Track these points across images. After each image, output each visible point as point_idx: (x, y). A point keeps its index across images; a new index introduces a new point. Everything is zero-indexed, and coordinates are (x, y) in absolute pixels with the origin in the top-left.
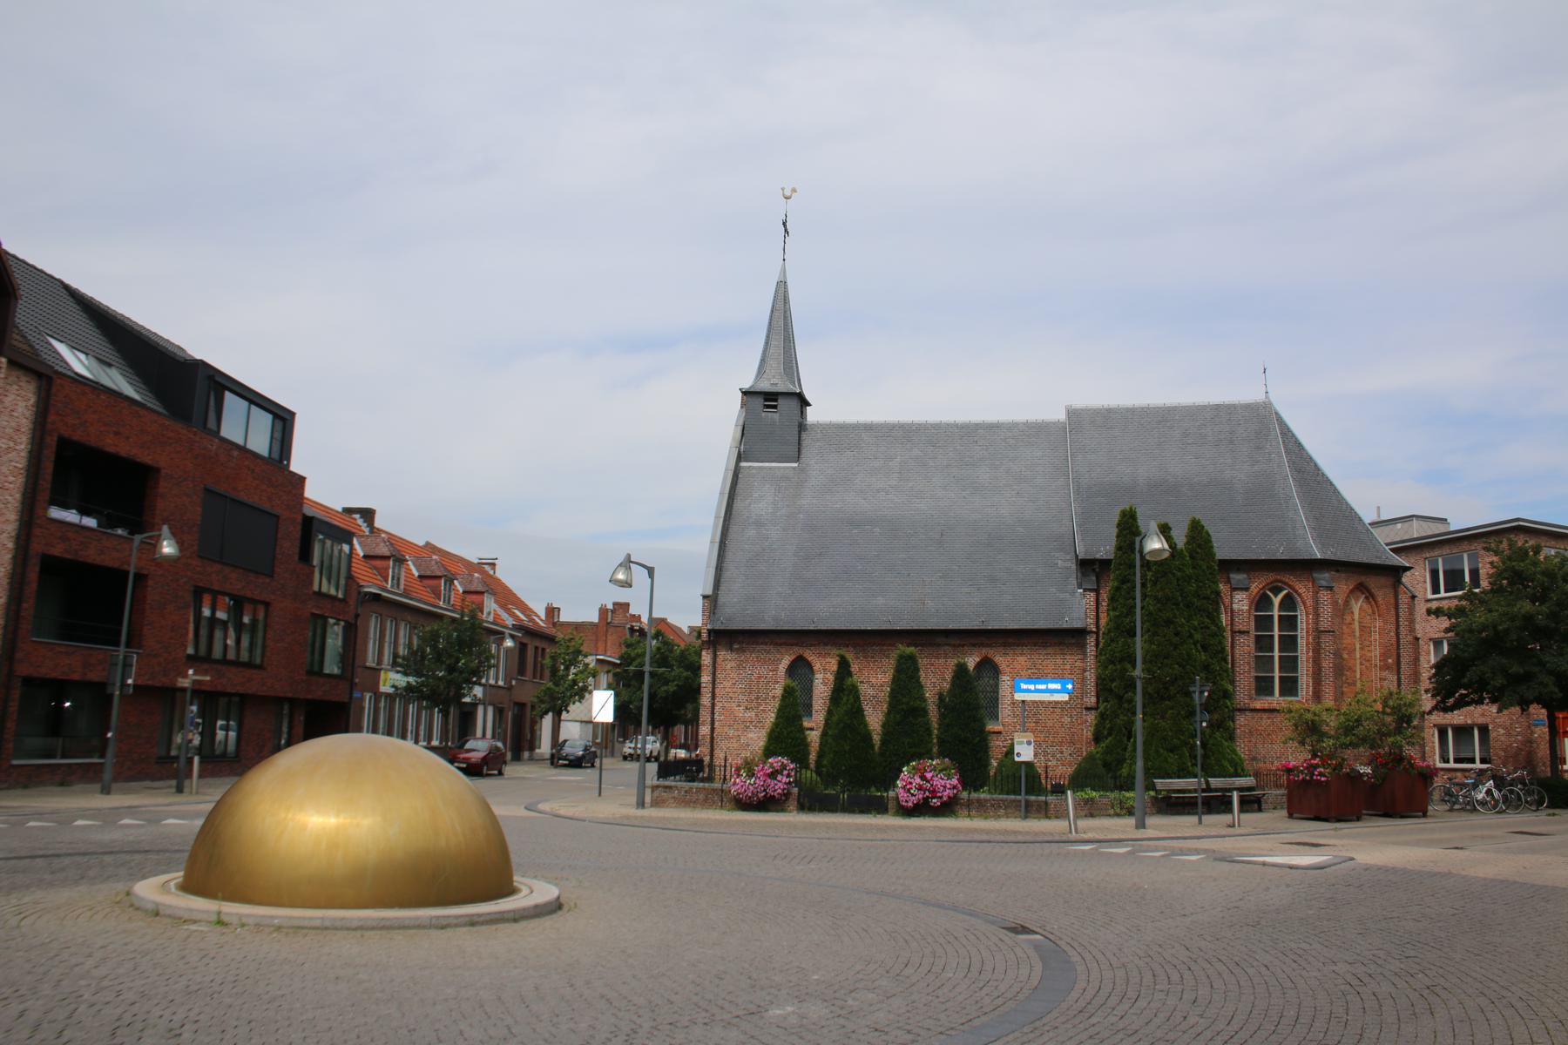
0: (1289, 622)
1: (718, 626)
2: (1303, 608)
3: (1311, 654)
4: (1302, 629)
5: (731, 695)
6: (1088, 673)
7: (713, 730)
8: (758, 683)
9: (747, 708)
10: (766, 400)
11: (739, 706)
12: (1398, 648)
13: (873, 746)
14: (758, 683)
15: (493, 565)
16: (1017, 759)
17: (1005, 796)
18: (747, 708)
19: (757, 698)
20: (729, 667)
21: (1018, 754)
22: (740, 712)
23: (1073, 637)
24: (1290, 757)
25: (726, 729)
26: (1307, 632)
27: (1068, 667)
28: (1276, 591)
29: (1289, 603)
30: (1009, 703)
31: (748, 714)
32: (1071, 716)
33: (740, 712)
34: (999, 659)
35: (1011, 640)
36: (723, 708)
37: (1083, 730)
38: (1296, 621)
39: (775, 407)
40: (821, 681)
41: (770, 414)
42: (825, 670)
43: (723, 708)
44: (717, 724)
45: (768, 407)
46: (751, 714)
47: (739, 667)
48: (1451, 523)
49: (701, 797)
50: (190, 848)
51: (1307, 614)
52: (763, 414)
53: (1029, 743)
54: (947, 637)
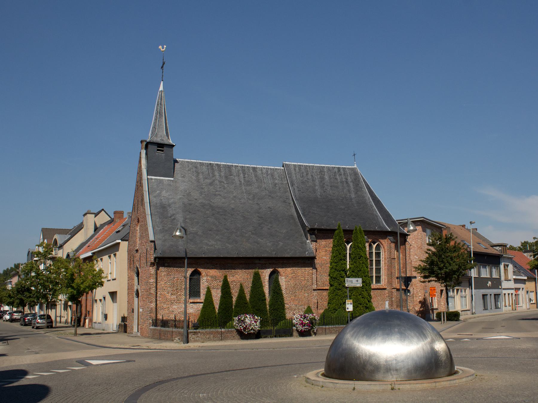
0: (378, 255)
1: (159, 255)
2: (383, 249)
3: (386, 267)
4: (383, 258)
5: (164, 288)
6: (314, 275)
7: (156, 305)
8: (177, 282)
9: (172, 294)
10: (158, 147)
11: (168, 293)
12: (406, 265)
13: (215, 312)
14: (177, 282)
15: (476, 229)
16: (347, 310)
17: (342, 326)
18: (172, 294)
19: (177, 289)
20: (163, 275)
21: (348, 308)
22: (169, 296)
23: (309, 260)
24: (380, 307)
25: (162, 304)
26: (385, 259)
27: (307, 273)
28: (374, 243)
29: (378, 248)
30: (284, 288)
31: (173, 297)
32: (308, 293)
33: (169, 296)
34: (201, 270)
35: (285, 262)
36: (161, 294)
37: (312, 299)
38: (380, 255)
39: (162, 151)
40: (206, 280)
41: (160, 154)
42: (207, 275)
43: (161, 294)
44: (158, 302)
45: (158, 150)
46: (174, 297)
47: (168, 275)
48: (408, 218)
49: (212, 336)
50: (325, 360)
51: (385, 252)
52: (157, 153)
53: (351, 304)
54: (260, 260)
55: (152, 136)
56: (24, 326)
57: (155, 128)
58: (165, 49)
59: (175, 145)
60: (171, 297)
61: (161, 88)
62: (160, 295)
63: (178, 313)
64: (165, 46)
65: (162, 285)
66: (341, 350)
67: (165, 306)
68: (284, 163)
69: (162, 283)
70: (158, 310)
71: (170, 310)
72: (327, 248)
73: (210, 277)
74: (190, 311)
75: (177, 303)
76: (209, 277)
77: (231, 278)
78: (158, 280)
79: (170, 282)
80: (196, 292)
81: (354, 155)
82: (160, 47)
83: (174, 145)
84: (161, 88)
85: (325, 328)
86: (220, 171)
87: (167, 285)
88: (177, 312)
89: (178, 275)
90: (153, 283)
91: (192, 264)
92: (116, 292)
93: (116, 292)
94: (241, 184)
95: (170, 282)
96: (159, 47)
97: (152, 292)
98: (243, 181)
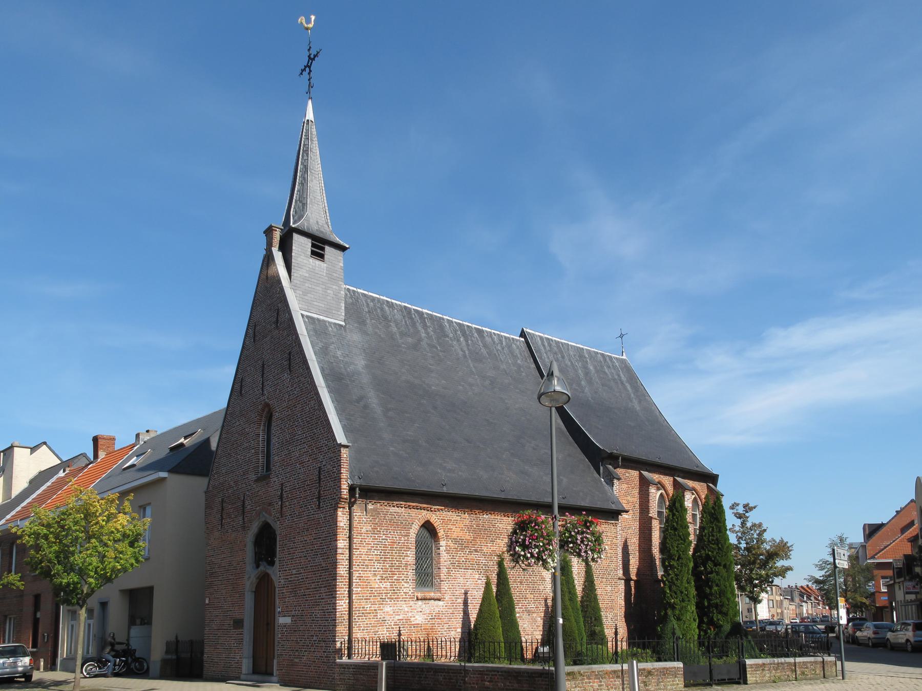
20: (364, 530)
33: (376, 583)
36: (360, 577)
40: (444, 548)
55: (296, 218)
56: (164, 676)
57: (301, 202)
58: (313, 23)
59: (348, 248)
60: (381, 584)
61: (310, 115)
62: (358, 581)
63: (394, 625)
64: (313, 18)
65: (362, 554)
66: (169, 657)
67: (369, 606)
68: (525, 329)
69: (364, 550)
70: (355, 617)
71: (379, 617)
72: (629, 498)
73: (452, 541)
74: (416, 619)
75: (393, 599)
76: (450, 542)
77: (489, 545)
78: (355, 542)
79: (379, 550)
80: (425, 575)
81: (621, 336)
82: (302, 20)
83: (347, 246)
84: (310, 115)
85: (795, 663)
86: (425, 327)
87: (372, 555)
88: (393, 622)
89: (394, 532)
90: (343, 548)
91: (421, 509)
92: (150, 590)
93: (150, 590)
94: (465, 356)
95: (379, 550)
96: (299, 20)
97: (342, 572)
98: (467, 352)
